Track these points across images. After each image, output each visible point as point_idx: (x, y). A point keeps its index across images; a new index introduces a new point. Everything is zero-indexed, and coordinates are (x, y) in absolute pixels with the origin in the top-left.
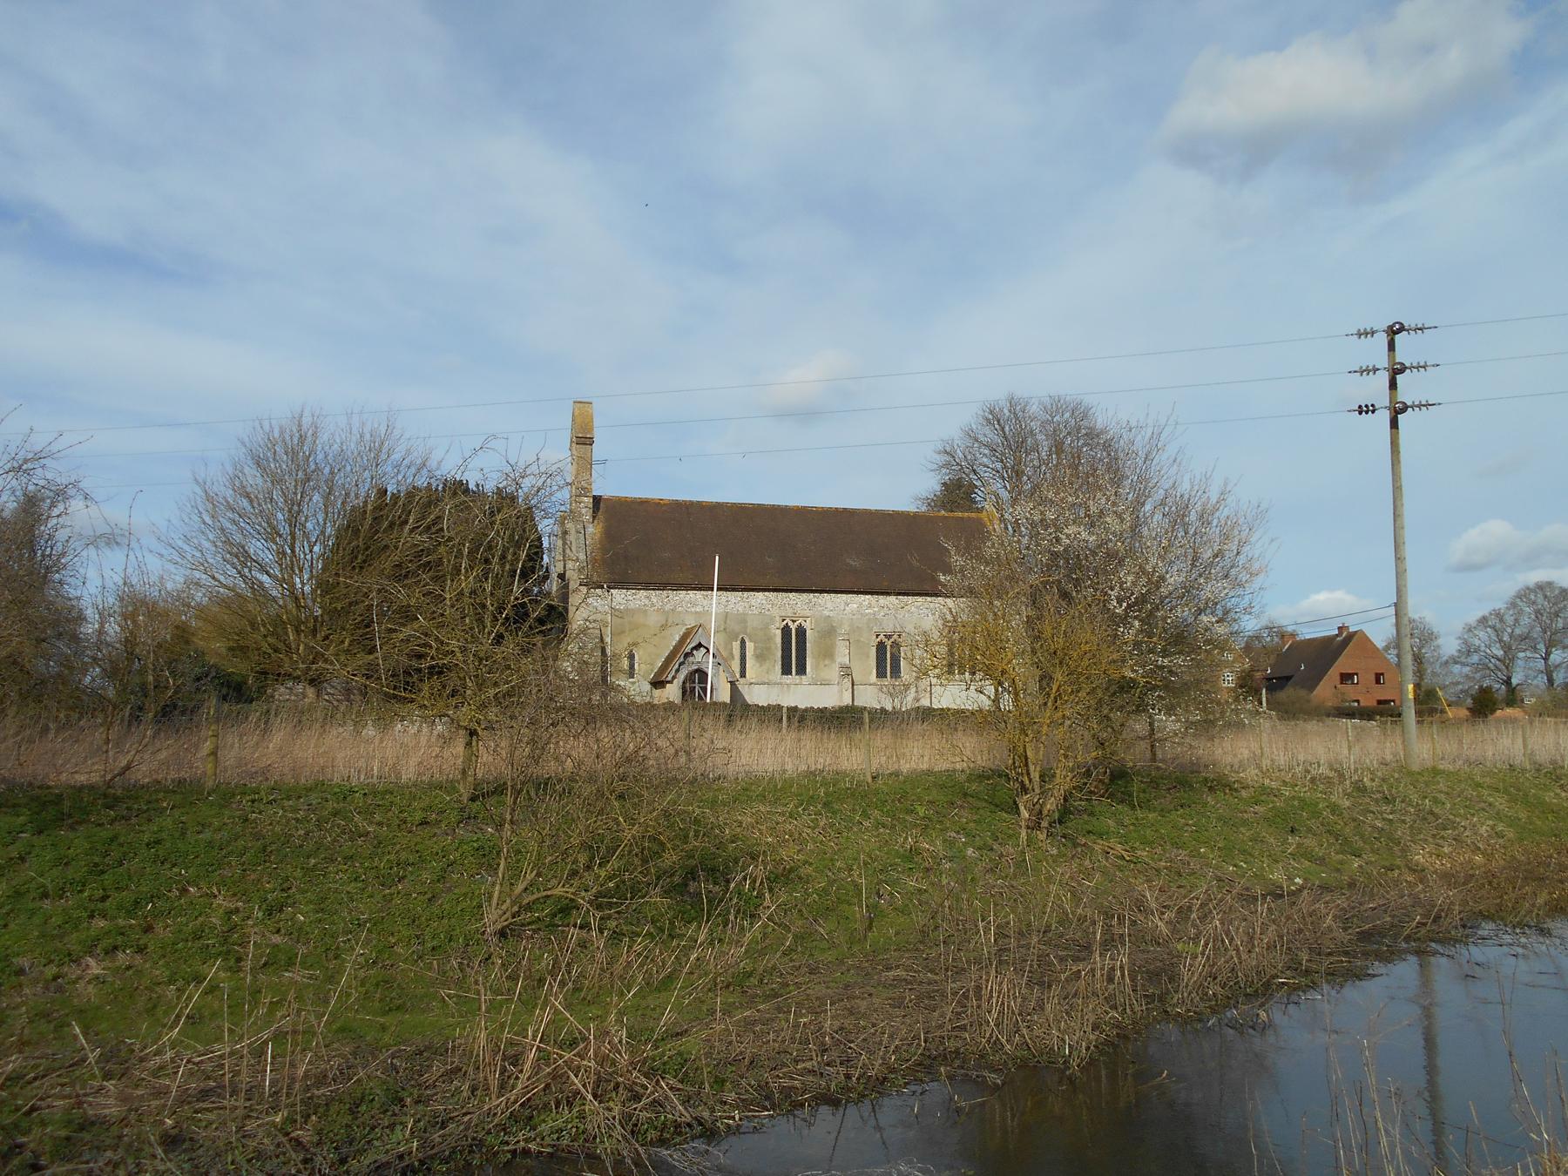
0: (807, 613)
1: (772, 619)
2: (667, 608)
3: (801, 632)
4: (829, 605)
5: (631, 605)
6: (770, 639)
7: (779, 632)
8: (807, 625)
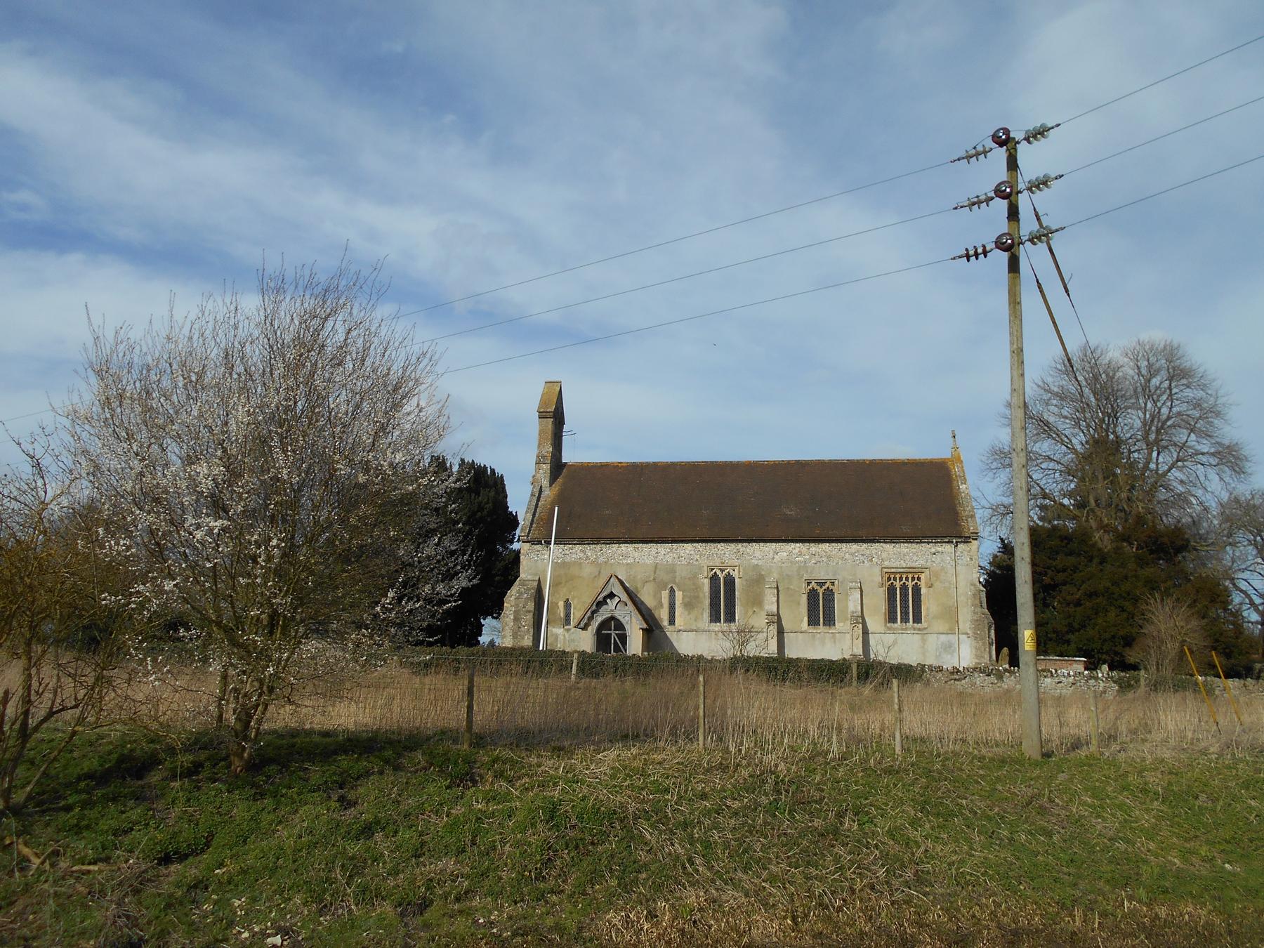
0: (736, 562)
1: (700, 568)
2: (601, 559)
3: (730, 582)
4: (758, 554)
5: (568, 559)
6: (698, 588)
7: (707, 581)
8: (735, 574)
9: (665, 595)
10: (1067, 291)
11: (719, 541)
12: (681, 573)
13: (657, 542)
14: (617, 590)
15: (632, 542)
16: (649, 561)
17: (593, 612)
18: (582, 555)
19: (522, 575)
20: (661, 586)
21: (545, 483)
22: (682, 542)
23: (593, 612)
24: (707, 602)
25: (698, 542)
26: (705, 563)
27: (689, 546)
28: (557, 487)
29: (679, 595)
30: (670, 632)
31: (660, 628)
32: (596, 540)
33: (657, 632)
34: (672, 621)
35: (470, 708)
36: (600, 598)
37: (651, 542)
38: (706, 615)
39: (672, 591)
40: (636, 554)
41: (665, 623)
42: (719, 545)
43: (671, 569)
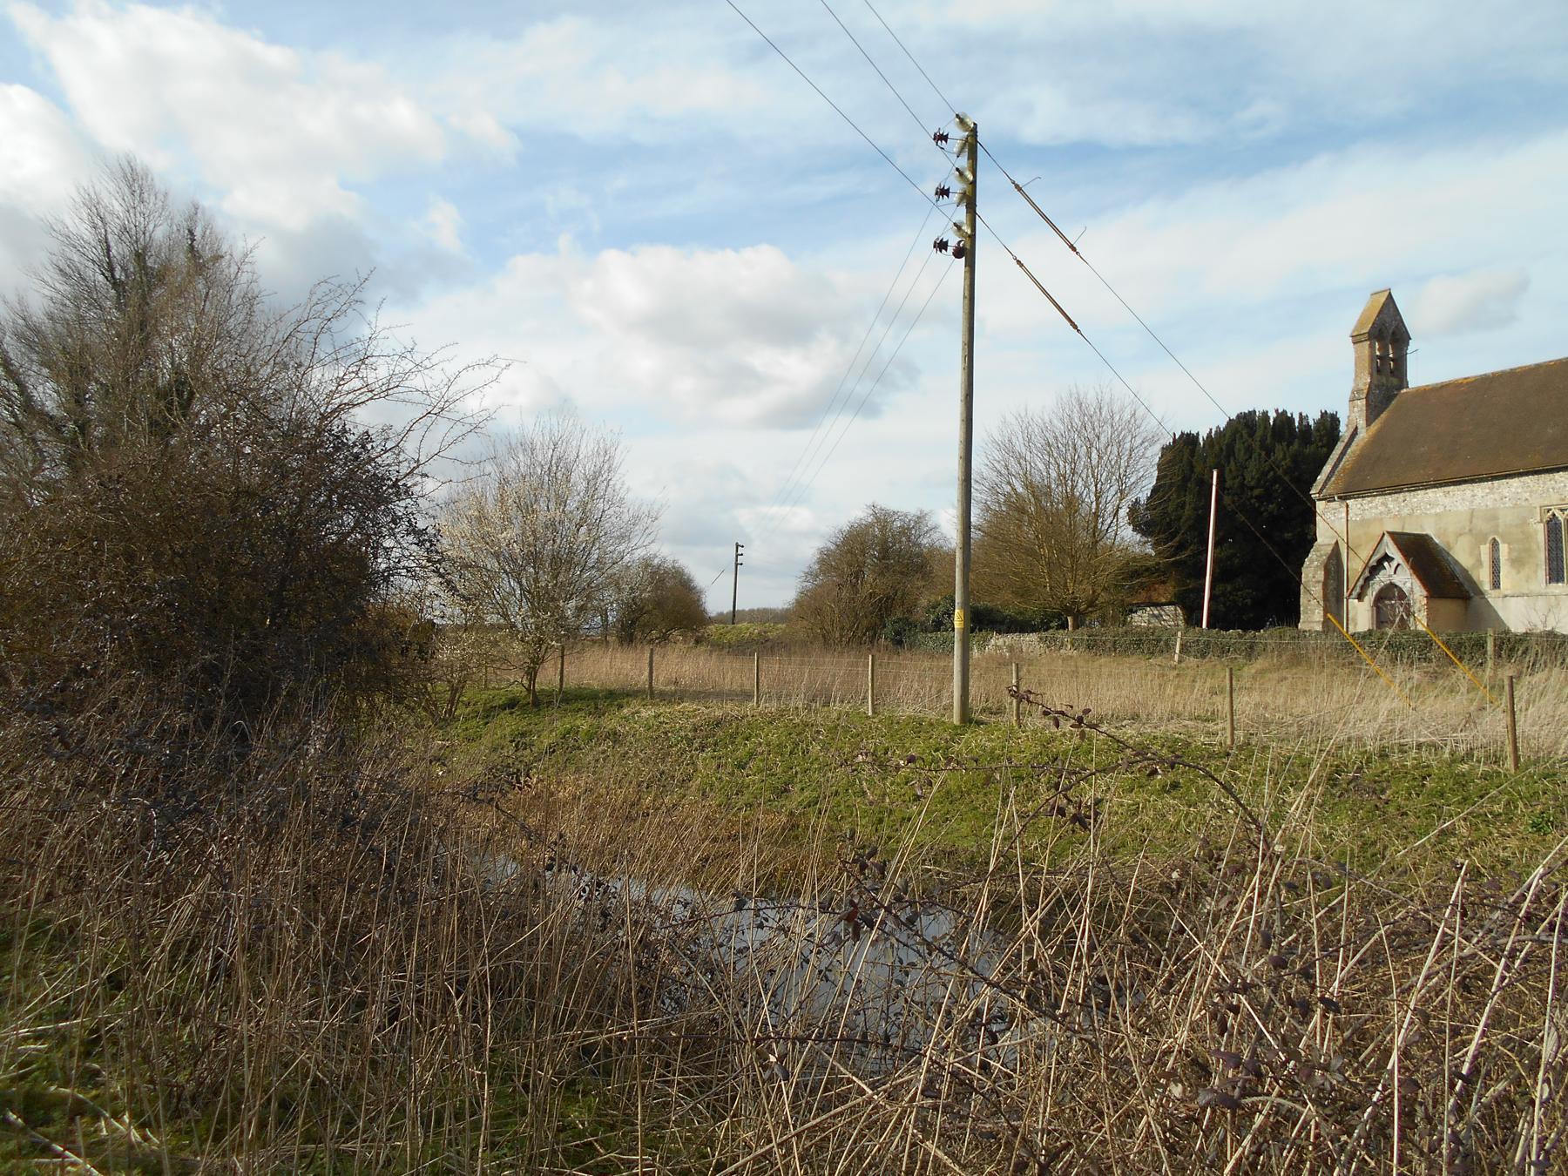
2: (1406, 511)
5: (1368, 515)
6: (1528, 537)
9: (1485, 550)
10: (1075, 327)
11: (1558, 470)
12: (1507, 519)
13: (1473, 481)
14: (1392, 550)
15: (1441, 485)
16: (1463, 507)
17: (1367, 580)
18: (1382, 508)
19: (1319, 540)
20: (1479, 539)
21: (1362, 422)
22: (1506, 477)
23: (1367, 580)
24: (1542, 556)
25: (1527, 474)
26: (1537, 502)
27: (1515, 482)
28: (1375, 426)
29: (1504, 549)
30: (1493, 597)
31: (1480, 593)
32: (1397, 489)
33: (1476, 598)
34: (1496, 584)
35: (1513, 704)
36: (1373, 562)
37: (1465, 482)
38: (1542, 573)
39: (1495, 544)
40: (1447, 501)
41: (1486, 586)
42: (1557, 476)
43: (1492, 516)
